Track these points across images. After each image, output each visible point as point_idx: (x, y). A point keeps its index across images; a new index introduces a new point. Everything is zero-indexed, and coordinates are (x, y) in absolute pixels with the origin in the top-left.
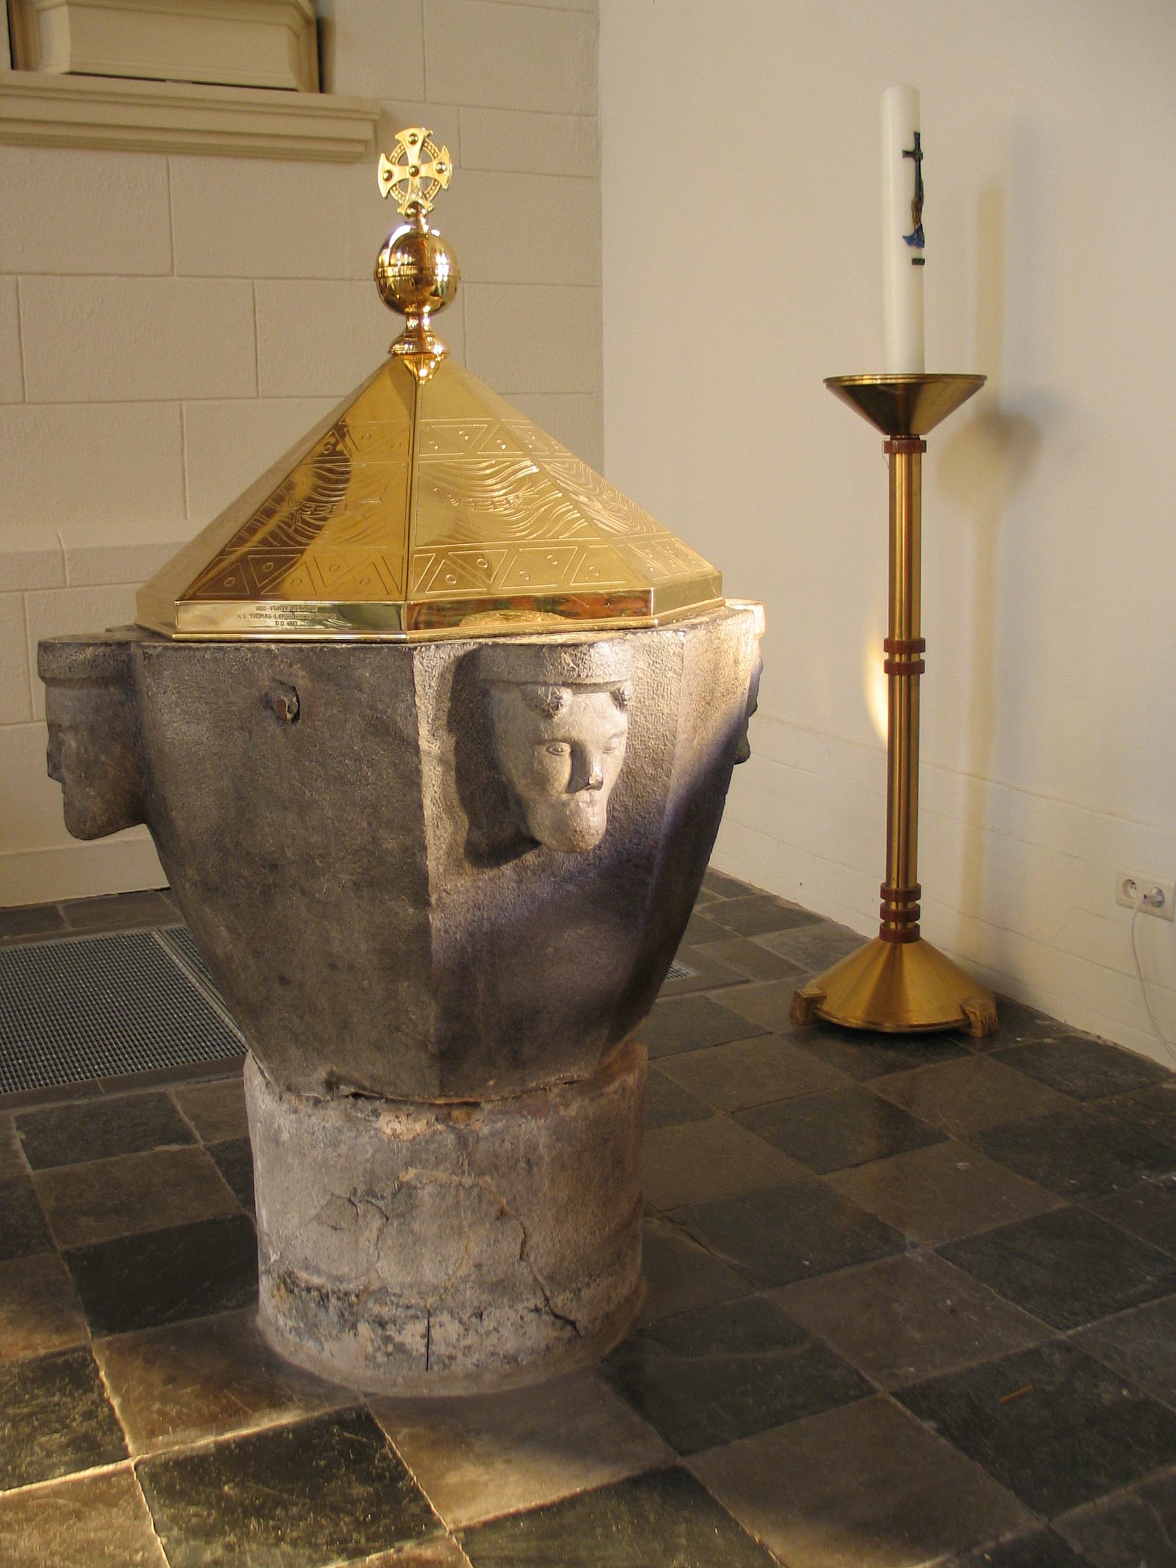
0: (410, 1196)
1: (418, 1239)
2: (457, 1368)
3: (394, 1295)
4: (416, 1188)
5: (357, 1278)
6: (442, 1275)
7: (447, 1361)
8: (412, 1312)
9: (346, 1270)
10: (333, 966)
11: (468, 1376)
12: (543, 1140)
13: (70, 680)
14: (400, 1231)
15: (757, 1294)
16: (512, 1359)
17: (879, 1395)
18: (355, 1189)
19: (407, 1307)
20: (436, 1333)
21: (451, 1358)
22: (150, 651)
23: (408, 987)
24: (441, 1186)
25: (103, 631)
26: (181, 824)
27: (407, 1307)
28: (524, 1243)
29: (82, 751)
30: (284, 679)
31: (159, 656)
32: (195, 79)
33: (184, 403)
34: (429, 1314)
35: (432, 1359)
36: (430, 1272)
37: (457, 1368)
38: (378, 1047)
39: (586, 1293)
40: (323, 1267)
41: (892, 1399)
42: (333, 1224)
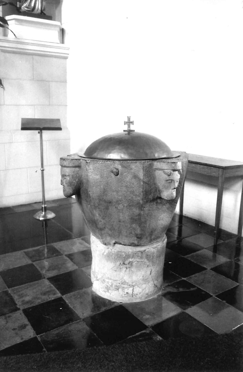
0: (132, 264)
1: (133, 272)
2: (138, 296)
3: (127, 283)
4: (133, 262)
5: (119, 280)
6: (136, 279)
7: (136, 295)
8: (130, 286)
9: (117, 279)
10: (120, 221)
11: (140, 298)
12: (155, 252)
13: (69, 166)
14: (129, 271)
15: (183, 279)
16: (147, 294)
17: (213, 297)
18: (121, 263)
19: (130, 285)
20: (135, 290)
21: (137, 294)
22: (87, 161)
23: (135, 225)
24: (138, 262)
25: (66, 156)
26: (91, 195)
27: (130, 285)
28: (151, 272)
29: (70, 180)
30: (116, 167)
31: (89, 162)
32: (34, 40)
33: (36, 106)
34: (134, 286)
35: (133, 295)
36: (135, 278)
37: (138, 296)
38: (126, 236)
39: (159, 280)
40: (112, 278)
41: (216, 297)
42: (115, 270)
